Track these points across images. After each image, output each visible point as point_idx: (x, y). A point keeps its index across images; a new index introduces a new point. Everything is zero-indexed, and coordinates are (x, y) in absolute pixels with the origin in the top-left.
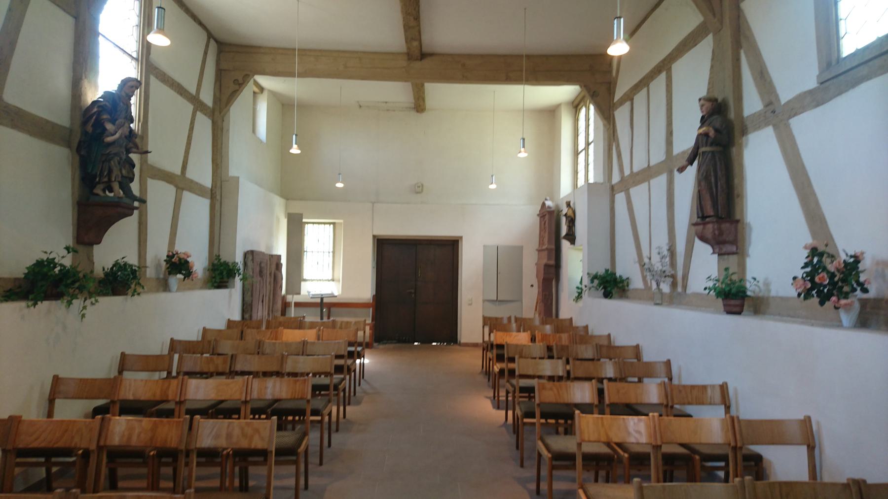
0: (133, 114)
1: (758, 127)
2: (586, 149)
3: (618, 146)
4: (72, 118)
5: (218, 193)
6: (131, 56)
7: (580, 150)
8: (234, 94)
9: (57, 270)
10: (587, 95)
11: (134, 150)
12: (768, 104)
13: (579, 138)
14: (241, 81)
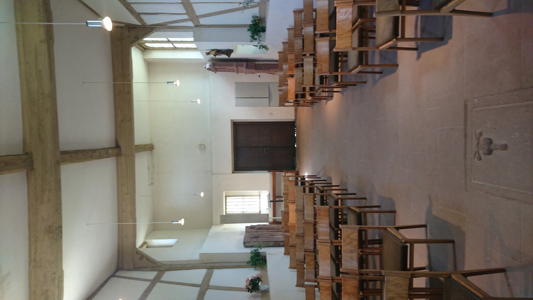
7: (173, 46)
8: (148, 259)
10: (138, 42)
14: (140, 256)
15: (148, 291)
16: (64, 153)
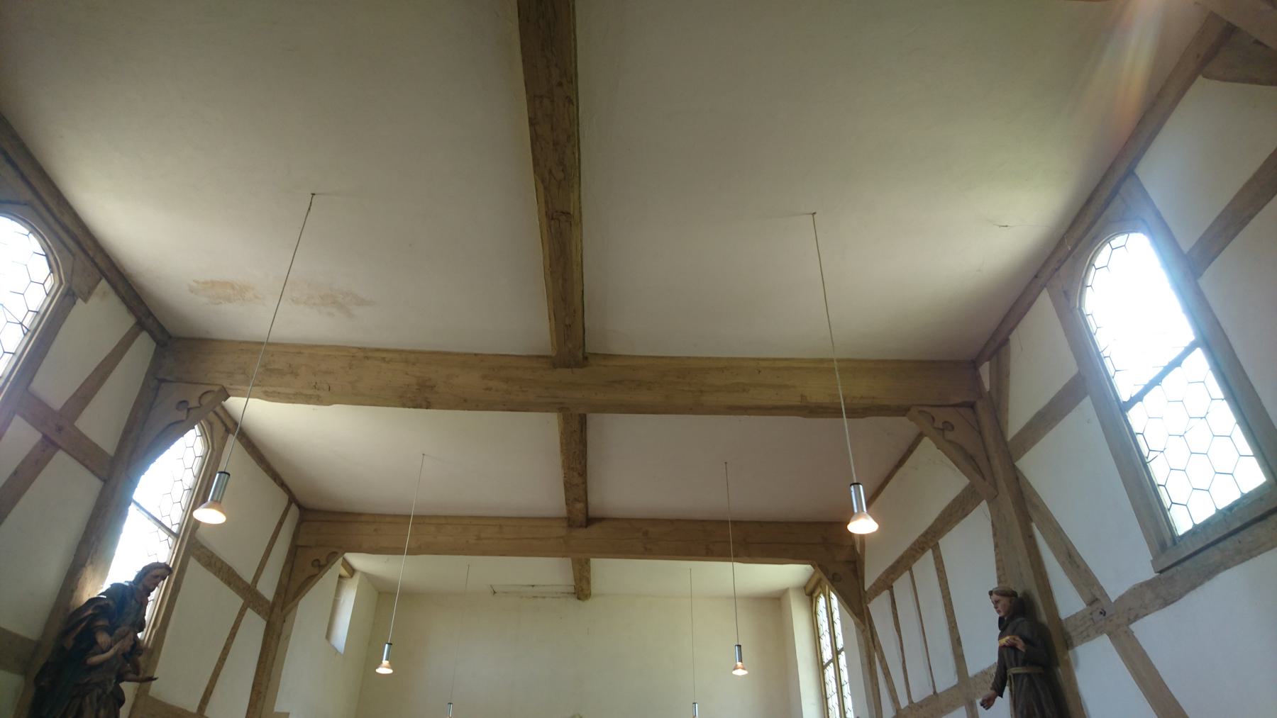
0: (146, 618)
1: (1087, 638)
2: (835, 660)
3: (882, 659)
6: (169, 530)
7: (826, 661)
8: (311, 580)
10: (825, 580)
11: (131, 676)
12: (1092, 602)
13: (830, 701)
14: (323, 562)
15: (228, 576)
16: (583, 420)
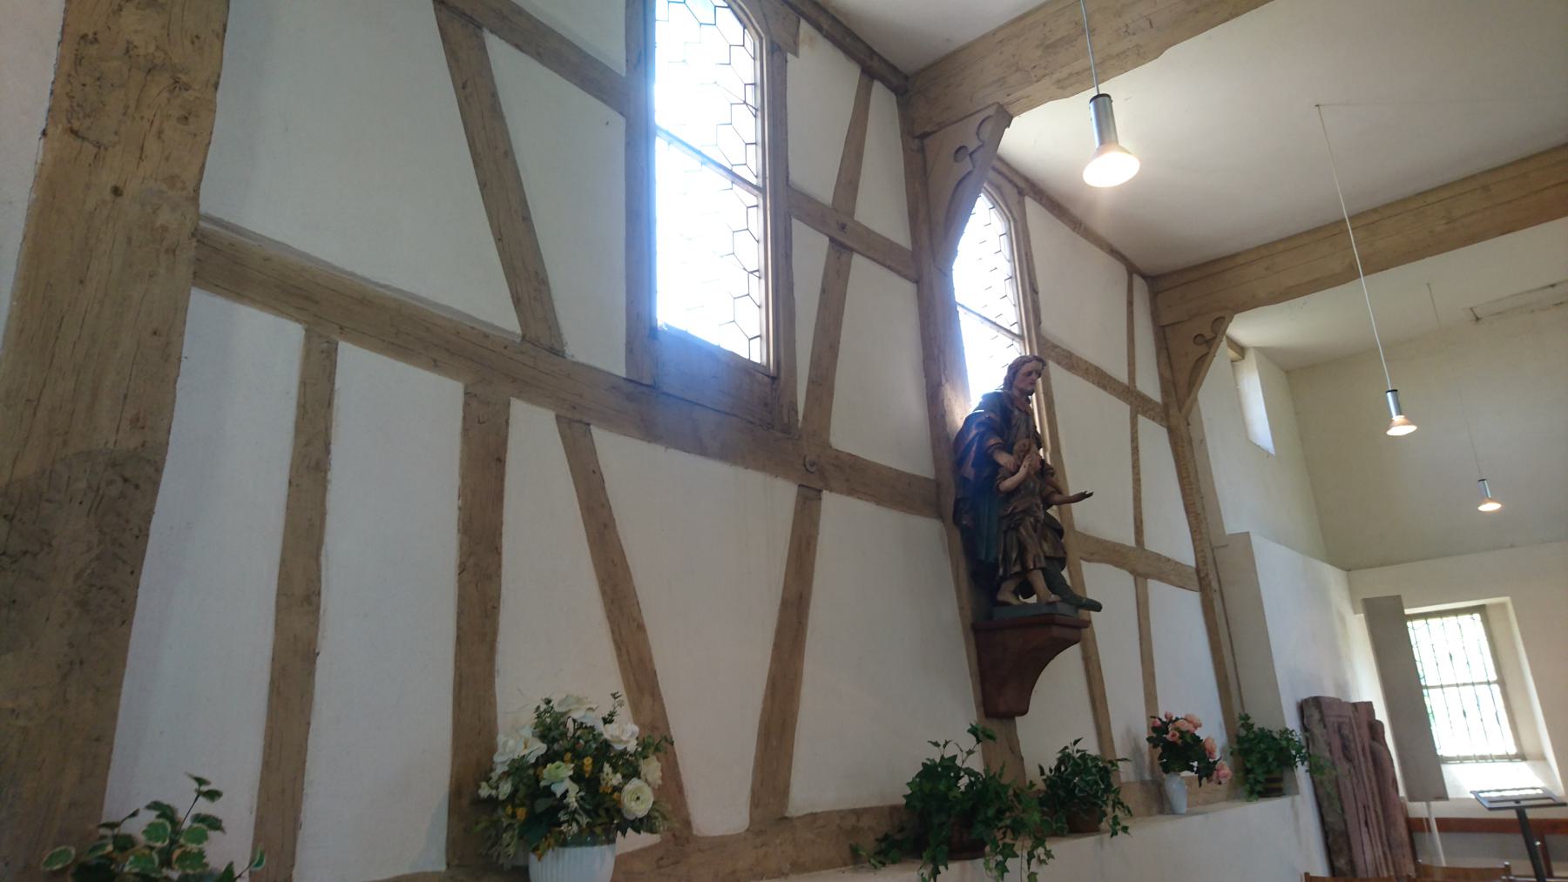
4: (936, 460)
5: (1212, 576)
9: (964, 782)
14: (1209, 335)
15: (1102, 379)
